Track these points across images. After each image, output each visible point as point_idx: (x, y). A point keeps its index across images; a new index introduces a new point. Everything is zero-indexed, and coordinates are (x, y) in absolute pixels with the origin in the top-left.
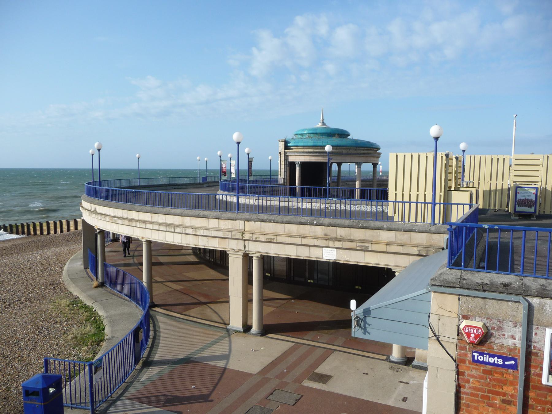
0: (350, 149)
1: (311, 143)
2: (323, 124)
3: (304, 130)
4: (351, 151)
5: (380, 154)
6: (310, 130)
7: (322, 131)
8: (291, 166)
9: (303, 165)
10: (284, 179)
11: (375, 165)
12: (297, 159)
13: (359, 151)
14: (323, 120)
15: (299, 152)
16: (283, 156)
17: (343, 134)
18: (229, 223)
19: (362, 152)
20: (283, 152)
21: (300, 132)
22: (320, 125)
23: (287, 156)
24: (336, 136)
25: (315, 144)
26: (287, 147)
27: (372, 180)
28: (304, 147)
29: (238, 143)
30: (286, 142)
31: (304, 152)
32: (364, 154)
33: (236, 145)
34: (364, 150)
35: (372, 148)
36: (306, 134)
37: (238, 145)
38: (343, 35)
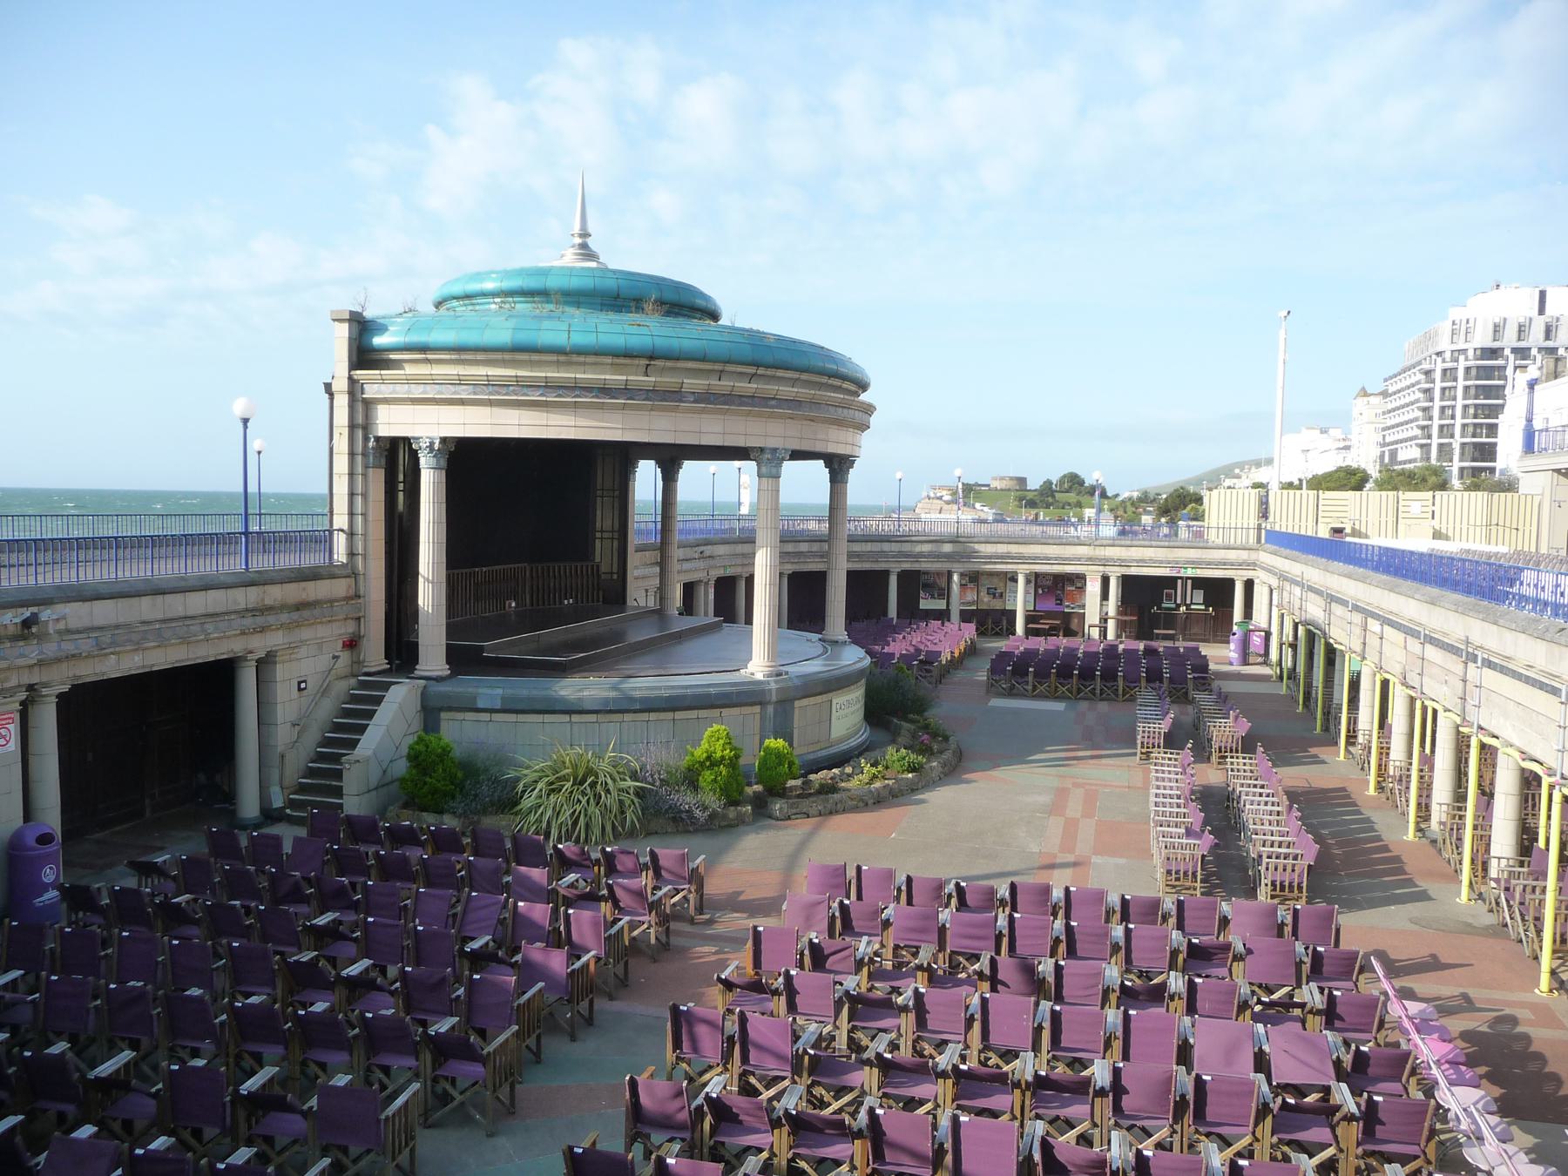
0: (721, 375)
1: (501, 334)
2: (586, 252)
3: (479, 276)
4: (726, 384)
5: (869, 409)
6: (507, 274)
7: (575, 283)
8: (395, 457)
9: (463, 456)
10: (351, 534)
11: (839, 466)
12: (426, 419)
13: (771, 388)
14: (585, 234)
15: (432, 381)
16: (342, 401)
17: (684, 304)
18: (1490, 505)
19: (787, 391)
20: (341, 385)
21: (457, 289)
22: (569, 258)
23: (369, 404)
24: (649, 307)
25: (524, 337)
26: (364, 356)
27: (828, 539)
28: (461, 352)
29: (245, 421)
30: (362, 327)
31: (460, 381)
32: (795, 403)
33: (241, 425)
34: (794, 382)
35: (844, 378)
36: (494, 294)
37: (246, 427)
38: (705, 105)
